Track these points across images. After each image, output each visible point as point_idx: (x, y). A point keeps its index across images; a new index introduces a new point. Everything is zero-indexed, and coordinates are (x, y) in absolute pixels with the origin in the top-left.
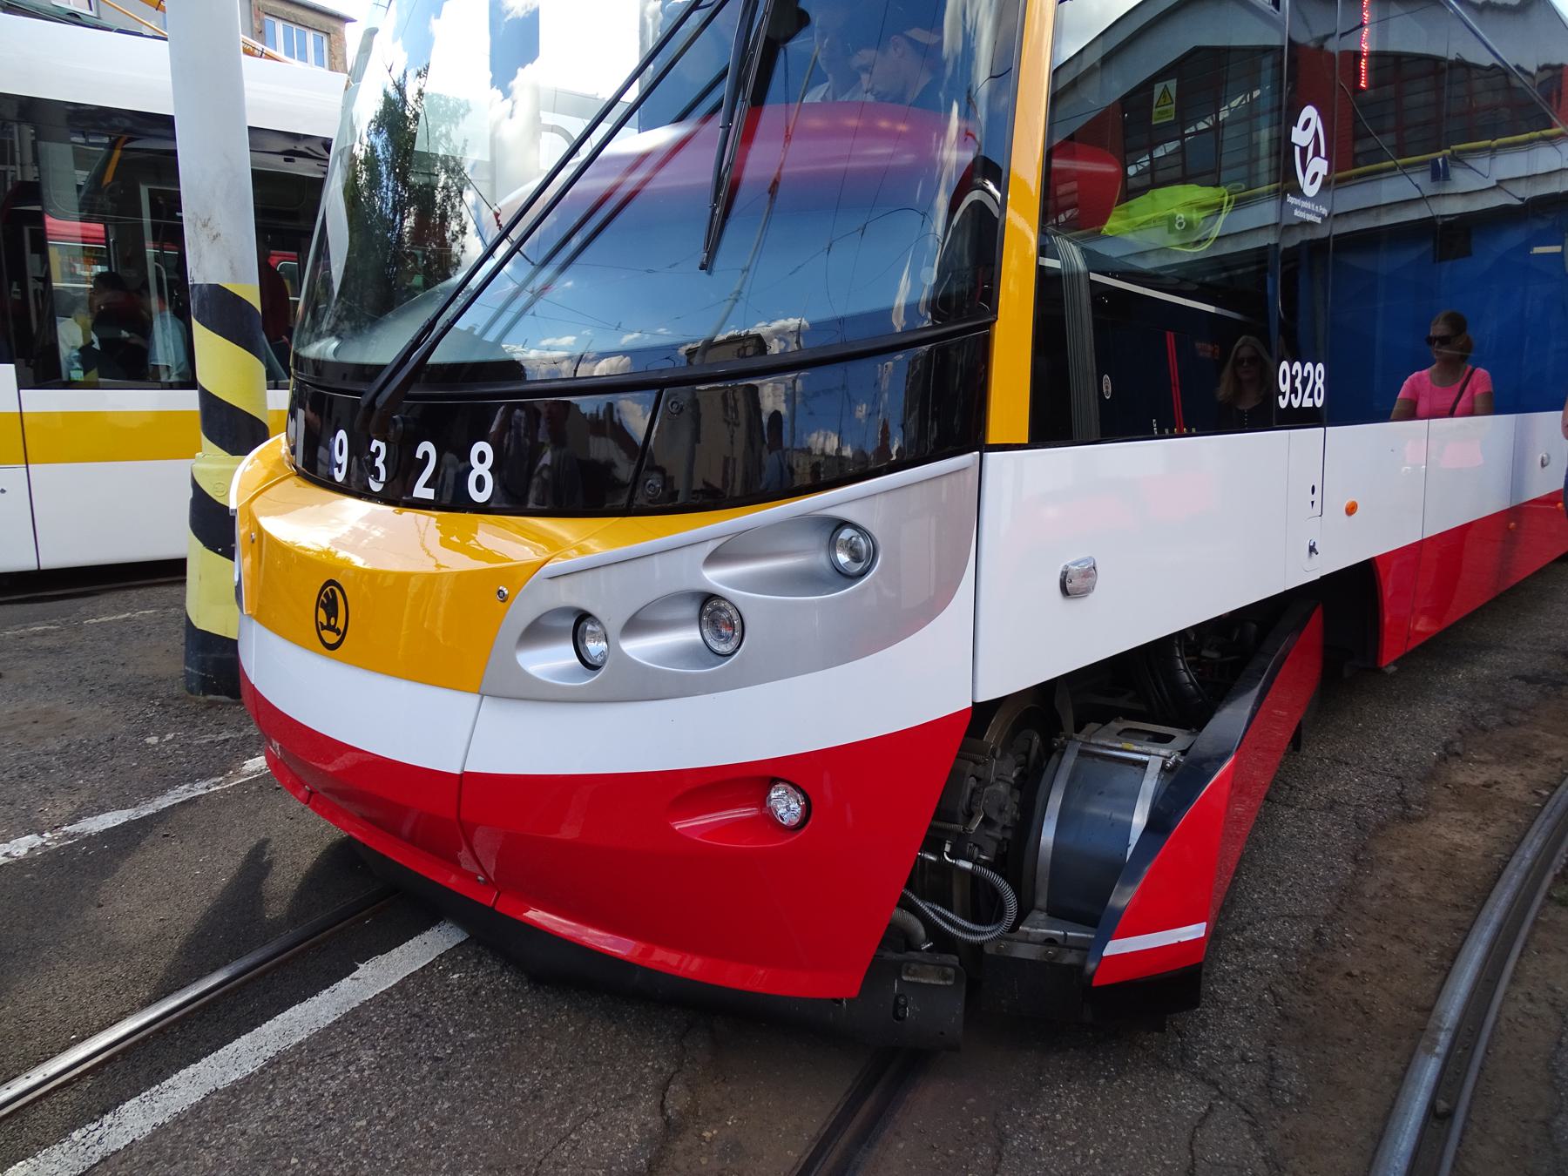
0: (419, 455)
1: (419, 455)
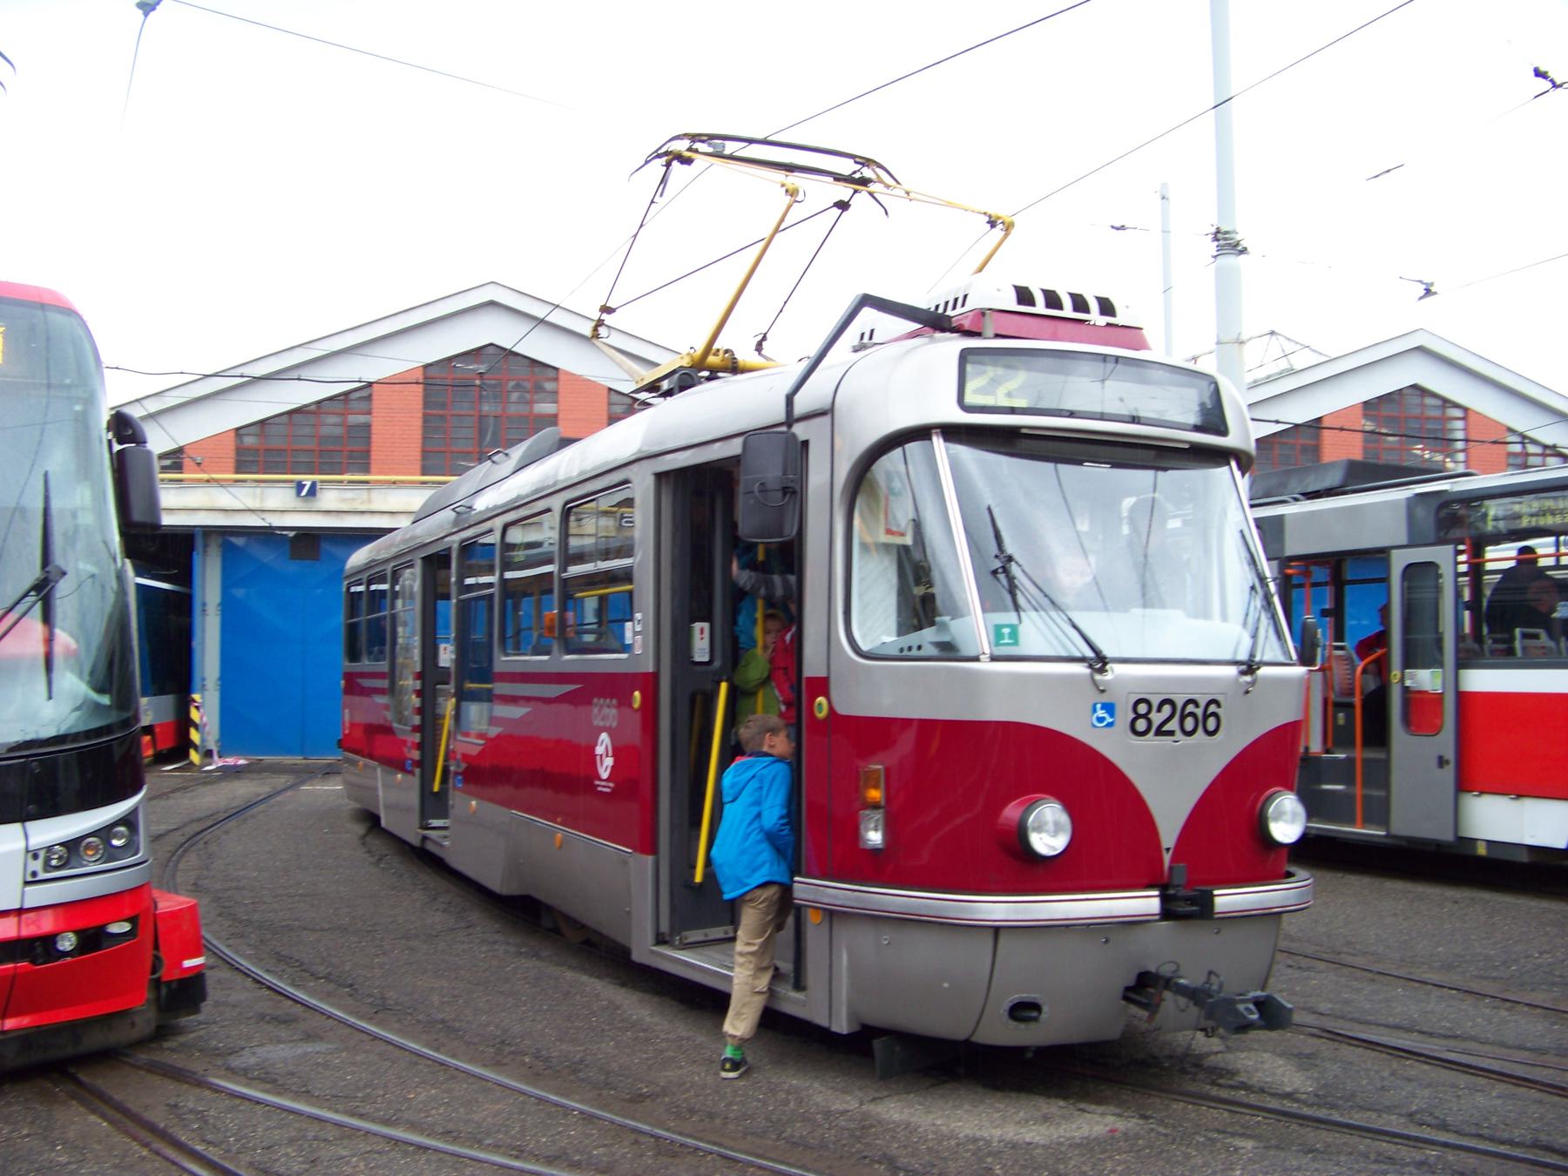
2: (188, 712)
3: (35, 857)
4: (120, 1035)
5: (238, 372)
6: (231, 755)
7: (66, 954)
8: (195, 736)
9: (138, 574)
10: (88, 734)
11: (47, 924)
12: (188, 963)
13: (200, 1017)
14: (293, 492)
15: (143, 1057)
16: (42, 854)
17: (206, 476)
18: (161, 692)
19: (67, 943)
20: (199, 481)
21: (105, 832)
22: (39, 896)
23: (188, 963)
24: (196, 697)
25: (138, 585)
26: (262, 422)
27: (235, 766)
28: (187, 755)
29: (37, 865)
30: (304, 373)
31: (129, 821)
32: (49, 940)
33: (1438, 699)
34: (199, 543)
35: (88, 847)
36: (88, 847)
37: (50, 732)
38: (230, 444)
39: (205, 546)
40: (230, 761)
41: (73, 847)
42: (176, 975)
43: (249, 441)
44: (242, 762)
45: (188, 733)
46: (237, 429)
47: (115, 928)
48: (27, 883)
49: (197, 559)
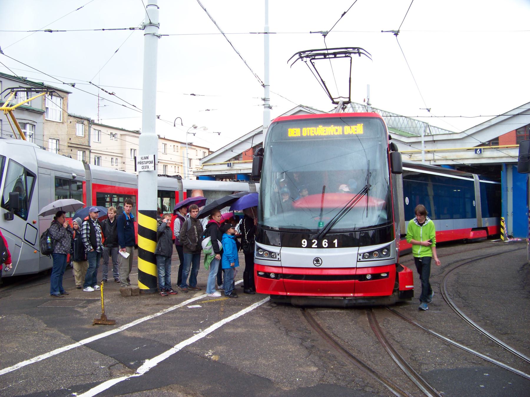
0: (313, 241)
1: (313, 241)
2: (500, 223)
3: (360, 255)
4: (386, 302)
5: (509, 114)
6: (516, 237)
7: (368, 280)
8: (502, 230)
9: (480, 179)
10: (380, 225)
11: (364, 272)
12: (407, 287)
13: (410, 301)
14: (474, 152)
15: (392, 309)
16: (362, 255)
17: (506, 146)
18: (491, 216)
19: (369, 277)
20: (504, 147)
21: (381, 250)
22: (360, 265)
23: (407, 287)
24: (503, 218)
25: (480, 182)
26: (525, 127)
27: (517, 241)
28: (499, 237)
29: (361, 257)
30: (447, 132)
31: (388, 248)
32: (365, 276)
33: (484, 216)
34: (504, 168)
35: (375, 254)
36: (375, 254)
37: (373, 225)
38: (514, 134)
39: (507, 169)
40: (515, 239)
41: (371, 253)
42: (403, 289)
43: (522, 133)
44: (519, 240)
45: (500, 230)
46: (516, 130)
47: (383, 275)
48: (357, 261)
49: (502, 173)
